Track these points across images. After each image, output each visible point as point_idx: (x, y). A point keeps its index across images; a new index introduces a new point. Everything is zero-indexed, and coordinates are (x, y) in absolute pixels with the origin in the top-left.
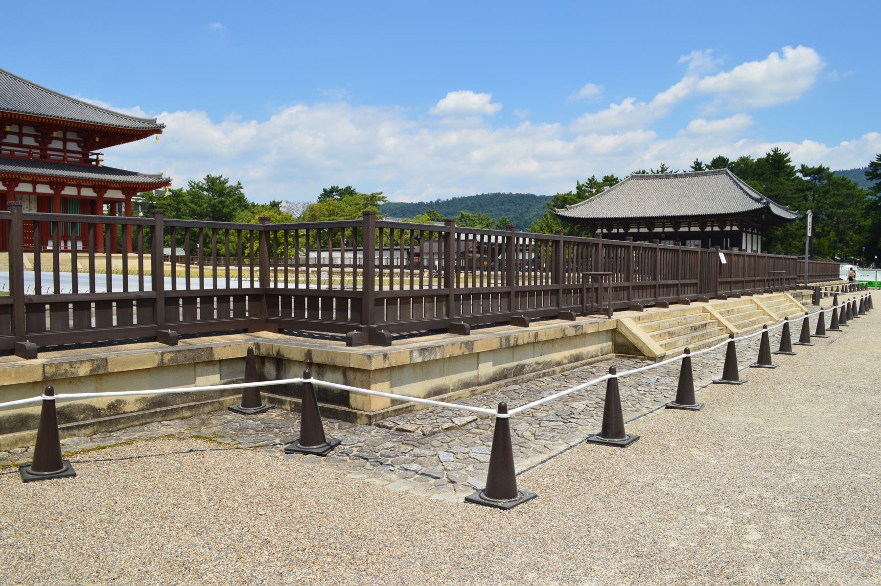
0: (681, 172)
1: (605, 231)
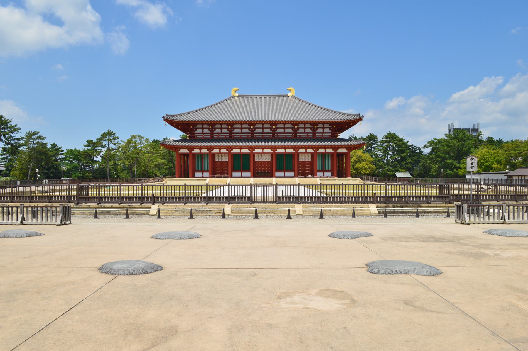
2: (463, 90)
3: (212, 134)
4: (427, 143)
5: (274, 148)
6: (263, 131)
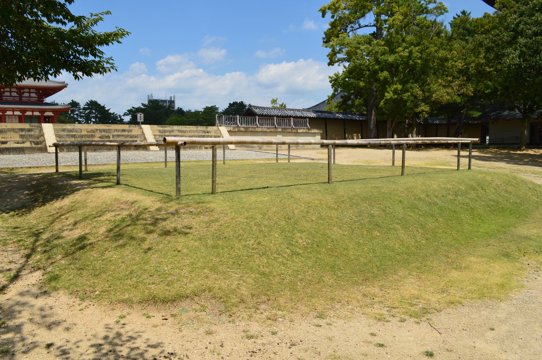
3: (20, 97)
4: (126, 111)
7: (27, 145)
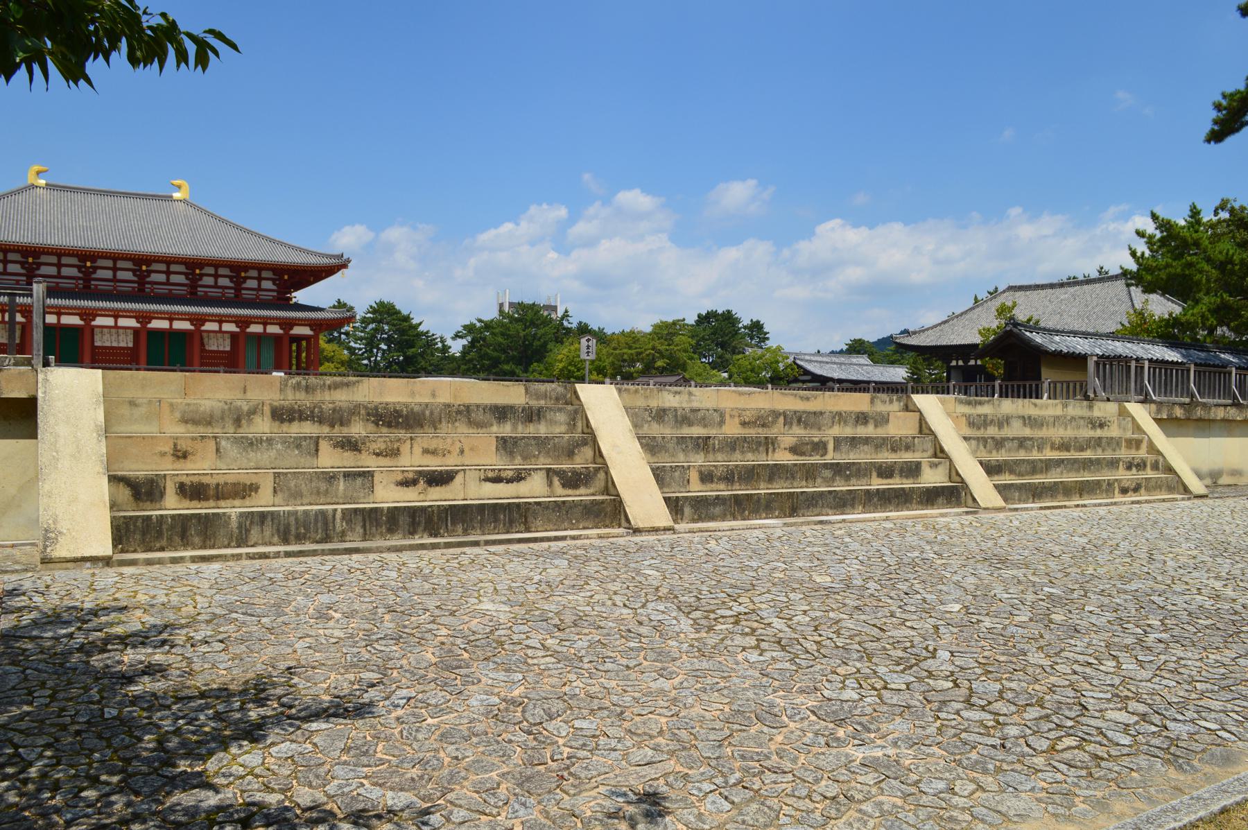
0: (1081, 278)
1: (961, 363)
2: (496, 227)
4: (461, 329)
5: (144, 318)
6: (115, 276)
7: (534, 489)
